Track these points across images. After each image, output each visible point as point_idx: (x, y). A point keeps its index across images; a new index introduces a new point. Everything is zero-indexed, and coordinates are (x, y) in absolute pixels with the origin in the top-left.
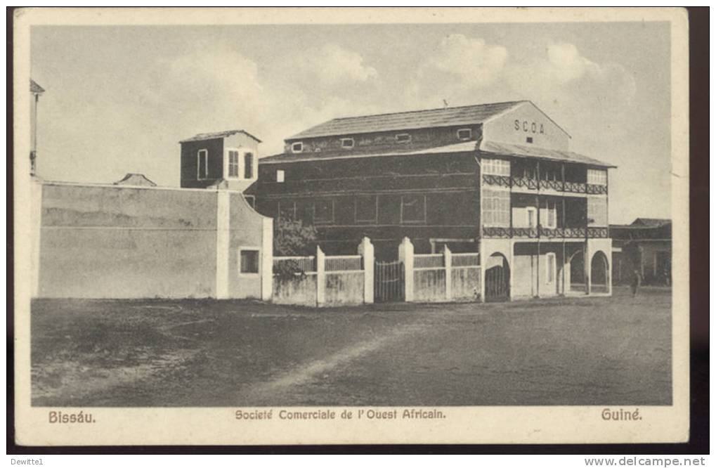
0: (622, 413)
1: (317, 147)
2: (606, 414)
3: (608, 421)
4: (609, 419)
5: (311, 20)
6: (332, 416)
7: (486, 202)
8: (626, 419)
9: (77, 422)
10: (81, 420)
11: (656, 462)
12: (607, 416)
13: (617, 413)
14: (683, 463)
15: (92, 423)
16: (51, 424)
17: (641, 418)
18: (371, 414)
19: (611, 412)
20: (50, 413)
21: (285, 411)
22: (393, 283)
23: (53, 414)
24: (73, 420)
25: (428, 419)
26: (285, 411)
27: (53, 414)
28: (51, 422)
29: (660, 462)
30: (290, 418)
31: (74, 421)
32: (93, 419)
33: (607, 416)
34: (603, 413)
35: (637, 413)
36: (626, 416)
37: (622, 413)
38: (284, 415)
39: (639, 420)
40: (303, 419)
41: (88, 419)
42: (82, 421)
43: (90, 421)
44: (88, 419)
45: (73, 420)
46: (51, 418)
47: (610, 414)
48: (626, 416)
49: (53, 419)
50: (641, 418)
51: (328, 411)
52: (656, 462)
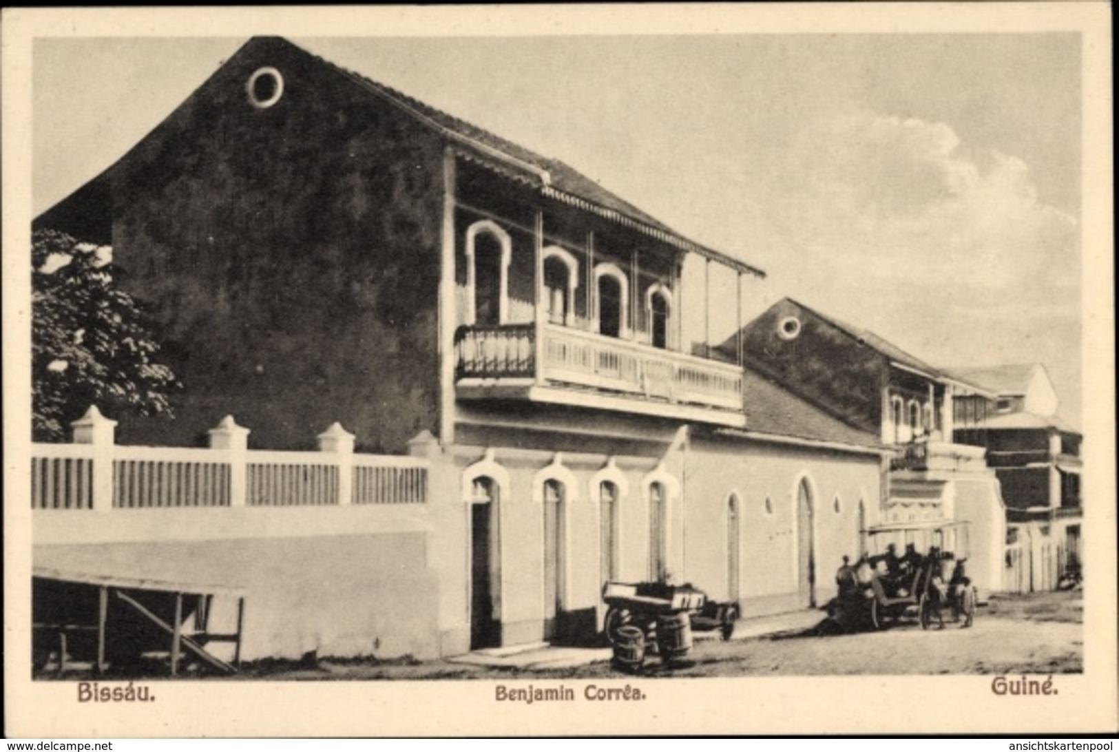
0: (562, 692)
1: (256, 363)
2: (999, 684)
3: (1002, 697)
4: (1004, 693)
5: (717, 30)
6: (570, 694)
7: (422, 409)
8: (1031, 692)
9: (508, 700)
10: (130, 697)
11: (70, 746)
12: (1001, 689)
13: (1018, 683)
14: (94, 748)
15: (149, 703)
16: (500, 702)
17: (1056, 692)
18: (592, 693)
19: (1008, 682)
20: (498, 688)
21: (593, 687)
22: (1046, 457)
23: (501, 690)
24: (106, 692)
25: (597, 701)
26: (593, 687)
27: (501, 690)
28: (81, 699)
29: (73, 746)
30: (601, 699)
31: (120, 699)
32: (150, 695)
33: (1001, 689)
34: (994, 681)
35: (1050, 684)
36: (1018, 688)
37: (1024, 684)
38: (592, 693)
39: (1052, 694)
40: (1042, 695)
41: (143, 695)
42: (133, 699)
43: (146, 699)
44: (143, 695)
45: (118, 697)
46: (498, 694)
47: (1005, 685)
48: (1018, 688)
49: (85, 695)
50: (1056, 692)
51: (531, 687)
52: (70, 746)
